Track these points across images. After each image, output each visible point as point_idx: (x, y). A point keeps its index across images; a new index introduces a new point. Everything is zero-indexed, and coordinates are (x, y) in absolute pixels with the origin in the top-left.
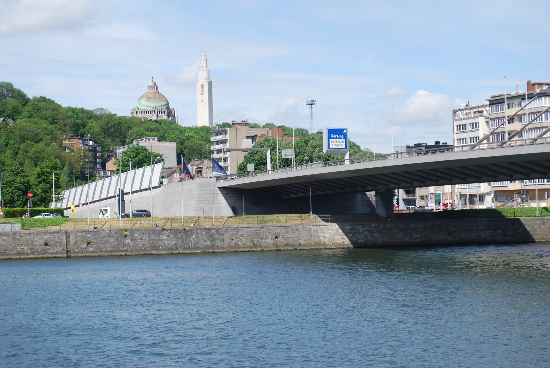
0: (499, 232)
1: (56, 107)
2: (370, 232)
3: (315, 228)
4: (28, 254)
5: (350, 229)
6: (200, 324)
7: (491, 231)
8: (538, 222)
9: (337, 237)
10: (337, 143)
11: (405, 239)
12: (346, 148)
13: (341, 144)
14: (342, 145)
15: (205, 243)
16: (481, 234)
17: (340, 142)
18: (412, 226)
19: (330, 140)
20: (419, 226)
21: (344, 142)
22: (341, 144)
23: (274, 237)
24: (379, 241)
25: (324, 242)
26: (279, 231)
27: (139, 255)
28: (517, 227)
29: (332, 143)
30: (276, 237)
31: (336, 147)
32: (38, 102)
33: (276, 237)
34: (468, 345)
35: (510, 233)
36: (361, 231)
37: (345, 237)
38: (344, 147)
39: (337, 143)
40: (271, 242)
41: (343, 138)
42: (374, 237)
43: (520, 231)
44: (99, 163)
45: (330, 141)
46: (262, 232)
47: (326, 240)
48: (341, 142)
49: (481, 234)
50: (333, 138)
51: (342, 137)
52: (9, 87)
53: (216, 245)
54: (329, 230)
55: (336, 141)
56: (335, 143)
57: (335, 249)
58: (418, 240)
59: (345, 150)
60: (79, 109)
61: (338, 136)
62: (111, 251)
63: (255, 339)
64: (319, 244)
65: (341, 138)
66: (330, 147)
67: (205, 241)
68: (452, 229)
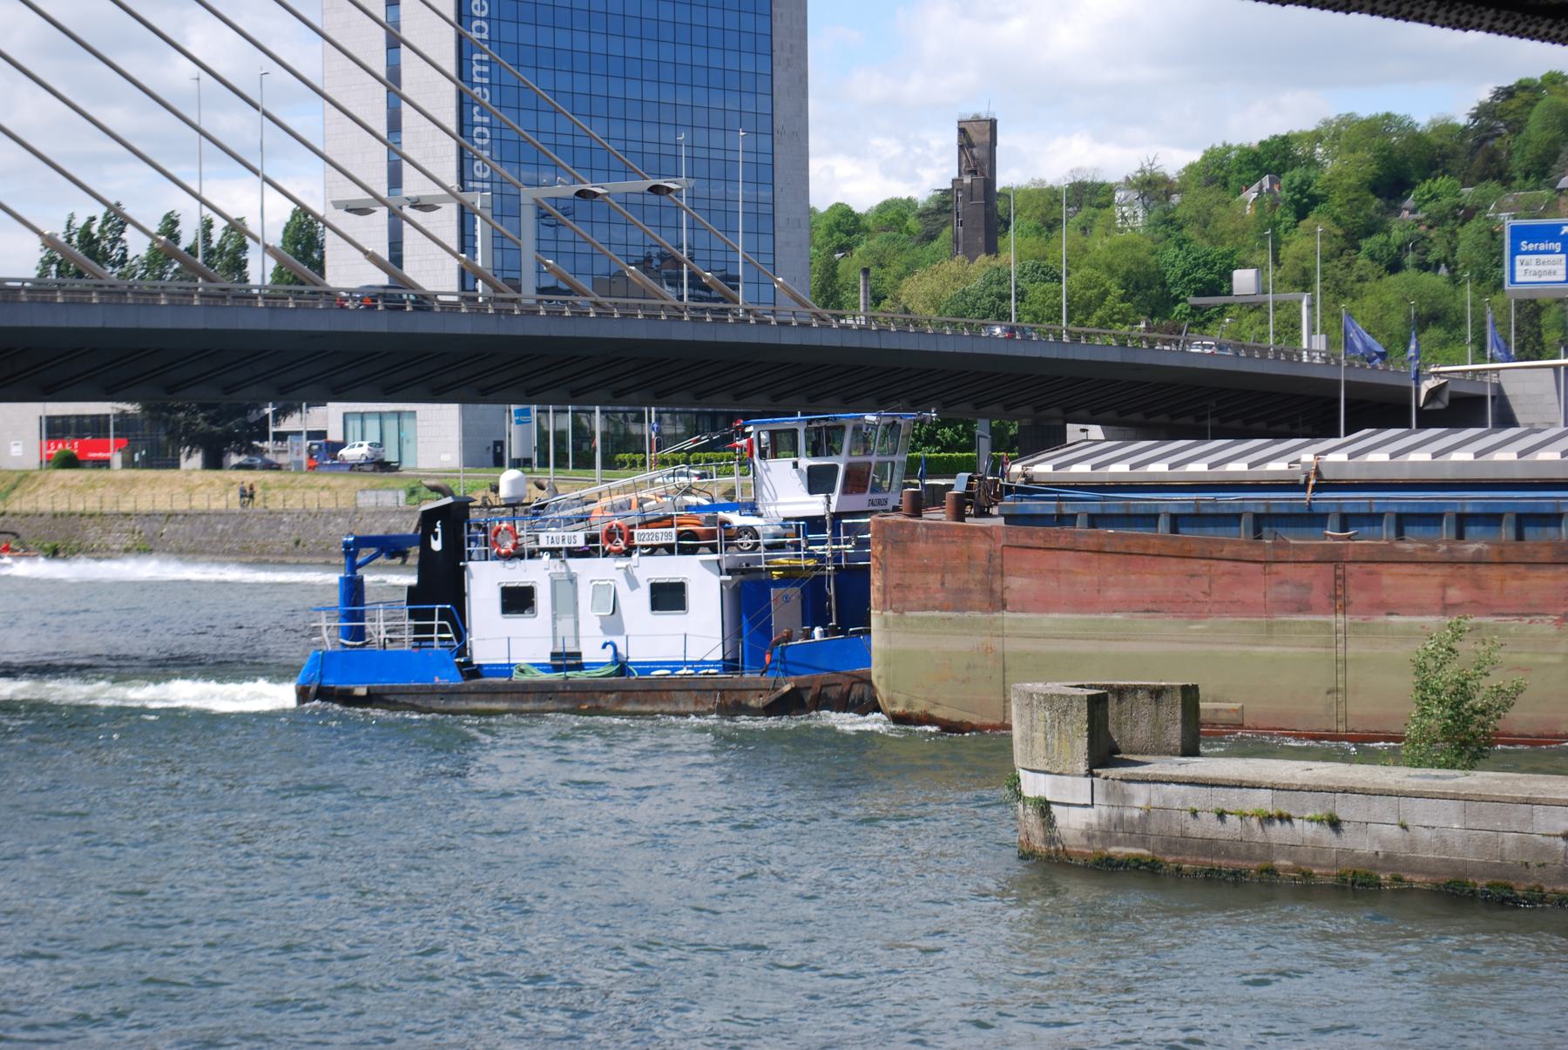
6: (296, 983)
13: (1553, 268)
14: (1555, 273)
17: (1549, 262)
19: (1518, 258)
22: (1553, 268)
32: (413, 207)
34: (1410, 1014)
41: (1559, 250)
45: (1518, 263)
48: (1554, 263)
50: (1527, 253)
52: (1564, 45)
55: (1538, 262)
56: (1533, 268)
57: (1507, 615)
60: (1241, 148)
61: (1542, 247)
63: (1025, 991)
65: (1552, 252)
66: (1518, 279)
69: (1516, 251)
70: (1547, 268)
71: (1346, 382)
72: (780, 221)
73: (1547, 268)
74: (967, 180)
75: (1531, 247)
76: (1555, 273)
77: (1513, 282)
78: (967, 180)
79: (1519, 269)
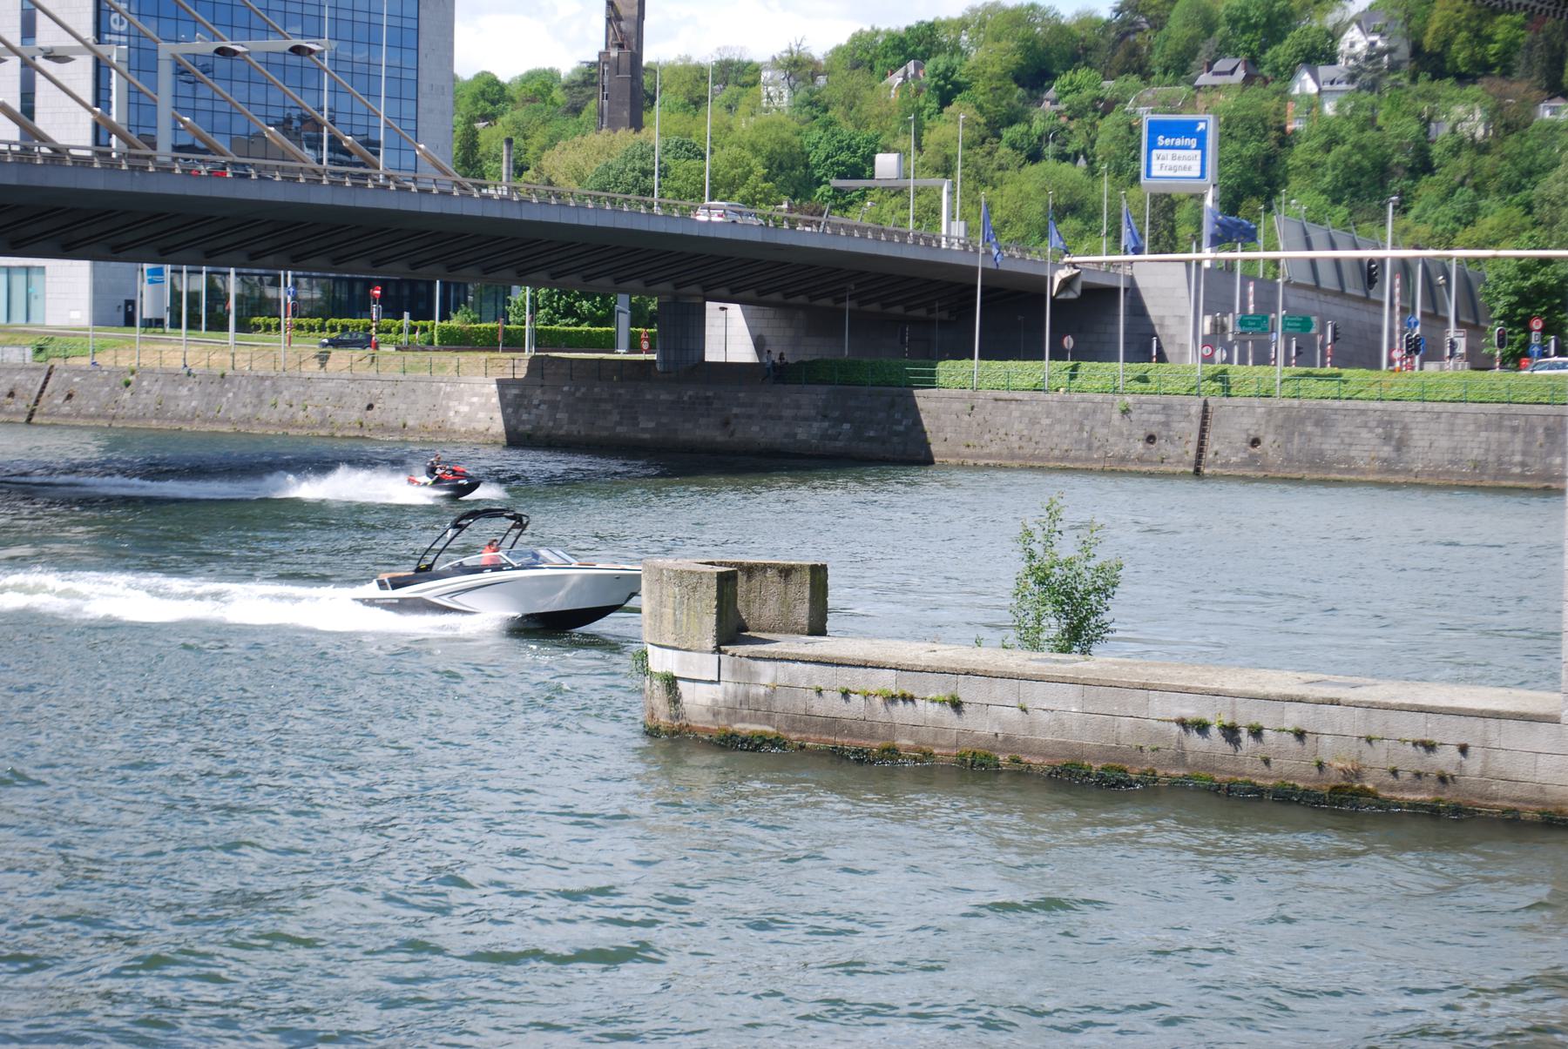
0: (846, 426)
1: (953, 21)
2: (554, 406)
3: (448, 389)
4: (1363, 472)
5: (516, 396)
7: (826, 424)
8: (957, 406)
9: (481, 415)
10: (1177, 163)
11: (619, 429)
12: (1202, 176)
13: (1188, 163)
15: (243, 411)
16: (799, 430)
17: (1184, 158)
18: (649, 397)
19: (1155, 152)
20: (664, 396)
21: (1199, 157)
22: (1188, 163)
23: (366, 405)
24: (562, 432)
25: (453, 424)
26: (378, 391)
27: (1340, 481)
28: (898, 416)
29: (1160, 162)
30: (370, 407)
31: (1171, 174)
33: (370, 407)
35: (872, 434)
36: (536, 402)
37: (498, 416)
38: (1198, 174)
39: (1177, 163)
40: (355, 415)
41: (1194, 146)
42: (555, 420)
43: (901, 428)
44: (1394, 194)
46: (348, 390)
47: (457, 420)
48: (1189, 159)
49: (799, 430)
50: (1163, 147)
51: (1193, 142)
53: (259, 416)
54: (475, 395)
55: (1174, 158)
56: (1168, 162)
58: (647, 436)
59: (1200, 182)
61: (1178, 142)
62: (92, 417)
64: (440, 429)
65: (1187, 148)
66: (1154, 173)
67: (245, 406)
68: (735, 410)
69: (1153, 145)
70: (1182, 163)
71: (983, 269)
72: (424, 87)
73: (1182, 163)
74: (614, 53)
75: (1168, 142)
76: (1190, 168)
77: (1149, 175)
78: (614, 53)
79: (1155, 164)
